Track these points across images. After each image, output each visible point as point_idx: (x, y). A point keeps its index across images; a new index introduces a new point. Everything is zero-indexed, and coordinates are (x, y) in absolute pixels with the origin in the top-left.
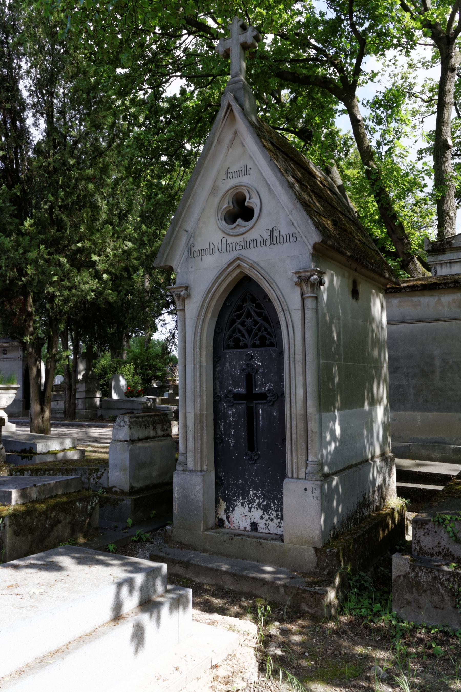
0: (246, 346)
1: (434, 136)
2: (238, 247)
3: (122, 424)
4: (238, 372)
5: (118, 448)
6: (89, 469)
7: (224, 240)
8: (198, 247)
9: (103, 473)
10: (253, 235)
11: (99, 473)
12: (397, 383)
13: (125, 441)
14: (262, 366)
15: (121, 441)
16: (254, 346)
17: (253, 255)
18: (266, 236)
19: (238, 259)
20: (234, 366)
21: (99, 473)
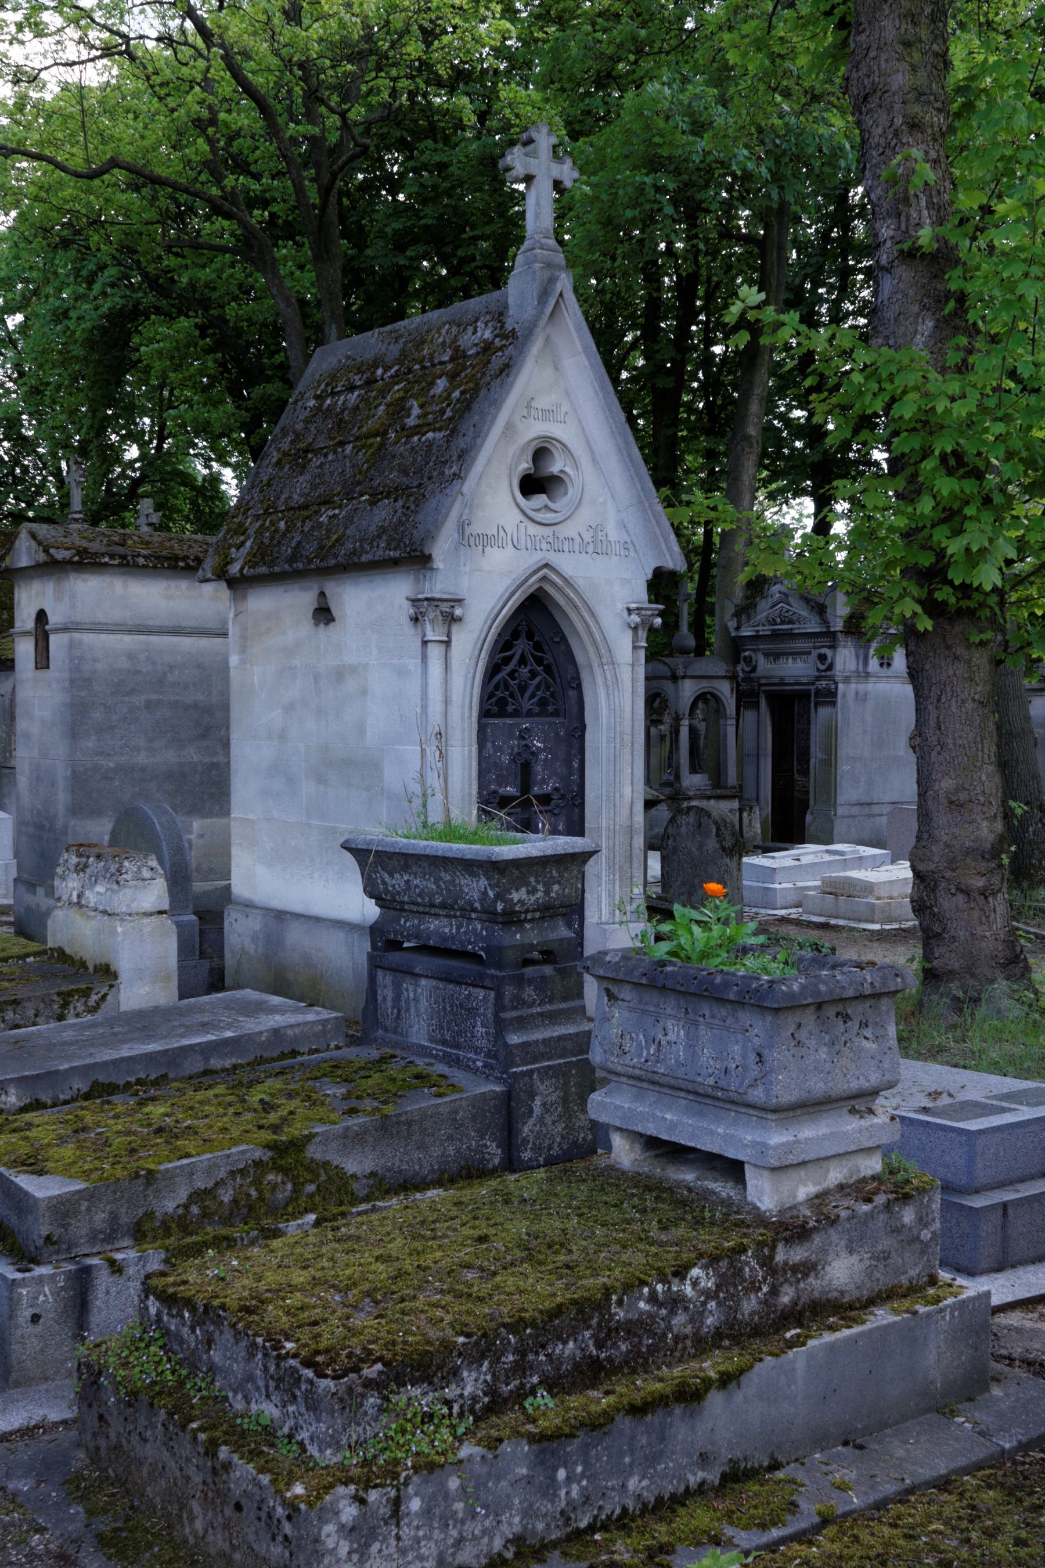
0: (516, 714)
1: (677, 308)
2: (544, 546)
3: (146, 873)
4: (506, 759)
5: (147, 930)
6: (59, 994)
7: (522, 526)
8: (476, 528)
9: (104, 997)
10: (569, 530)
11: (94, 998)
12: (207, 760)
13: (160, 912)
14: (544, 750)
15: (151, 914)
16: (530, 714)
17: (569, 565)
18: (587, 537)
19: (547, 565)
20: (500, 749)
21: (94, 998)
